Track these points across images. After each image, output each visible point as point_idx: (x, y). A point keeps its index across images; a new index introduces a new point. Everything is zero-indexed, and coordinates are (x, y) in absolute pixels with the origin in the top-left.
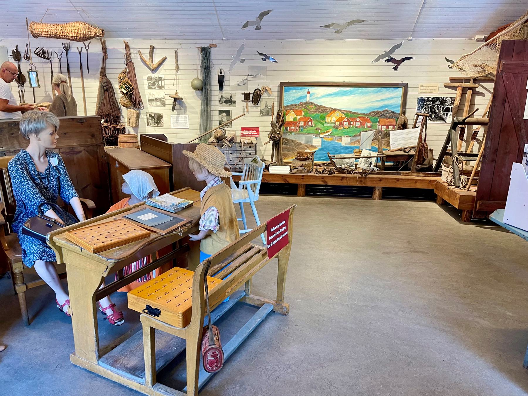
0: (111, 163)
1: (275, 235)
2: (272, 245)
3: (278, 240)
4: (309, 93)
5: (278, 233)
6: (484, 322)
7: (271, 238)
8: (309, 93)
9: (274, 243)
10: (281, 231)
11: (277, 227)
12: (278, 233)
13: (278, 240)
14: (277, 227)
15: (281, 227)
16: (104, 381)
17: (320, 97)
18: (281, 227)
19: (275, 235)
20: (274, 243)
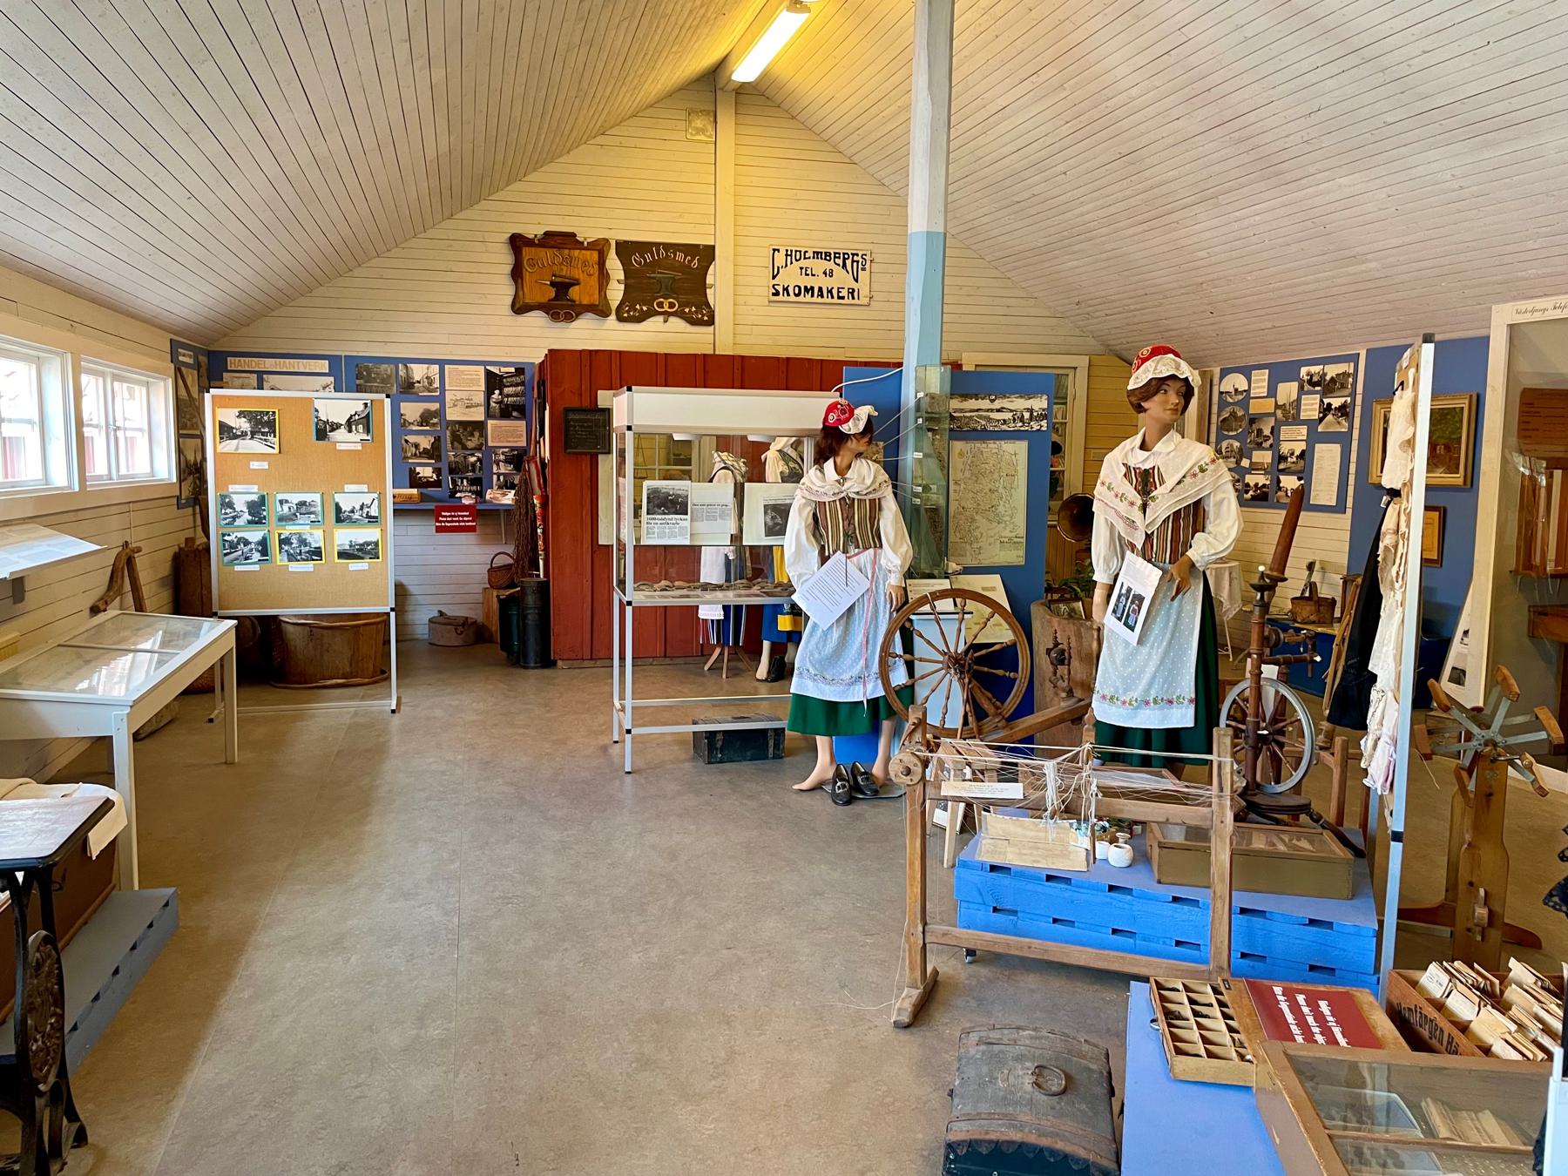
0: (1526, 640)
1: (1306, 1010)
2: (1281, 998)
3: (1290, 1018)
4: (1132, 504)
5: (1310, 1020)
6: (208, 289)
7: (1301, 998)
8: (1132, 504)
9: (1284, 1006)
10: (1316, 1030)
11: (1330, 1018)
12: (1310, 1020)
13: (1290, 1018)
14: (1330, 1018)
15: (1327, 1032)
16: (1031, 981)
17: (444, 148)
18: (1327, 1032)
19: (1306, 1010)
20: (1284, 1006)
